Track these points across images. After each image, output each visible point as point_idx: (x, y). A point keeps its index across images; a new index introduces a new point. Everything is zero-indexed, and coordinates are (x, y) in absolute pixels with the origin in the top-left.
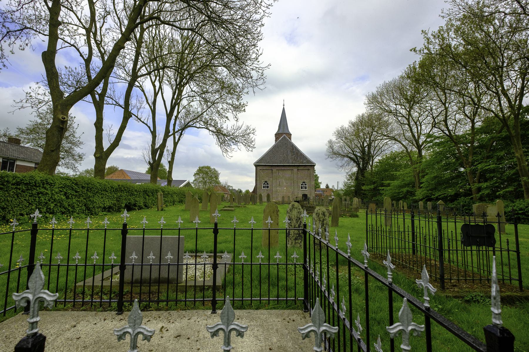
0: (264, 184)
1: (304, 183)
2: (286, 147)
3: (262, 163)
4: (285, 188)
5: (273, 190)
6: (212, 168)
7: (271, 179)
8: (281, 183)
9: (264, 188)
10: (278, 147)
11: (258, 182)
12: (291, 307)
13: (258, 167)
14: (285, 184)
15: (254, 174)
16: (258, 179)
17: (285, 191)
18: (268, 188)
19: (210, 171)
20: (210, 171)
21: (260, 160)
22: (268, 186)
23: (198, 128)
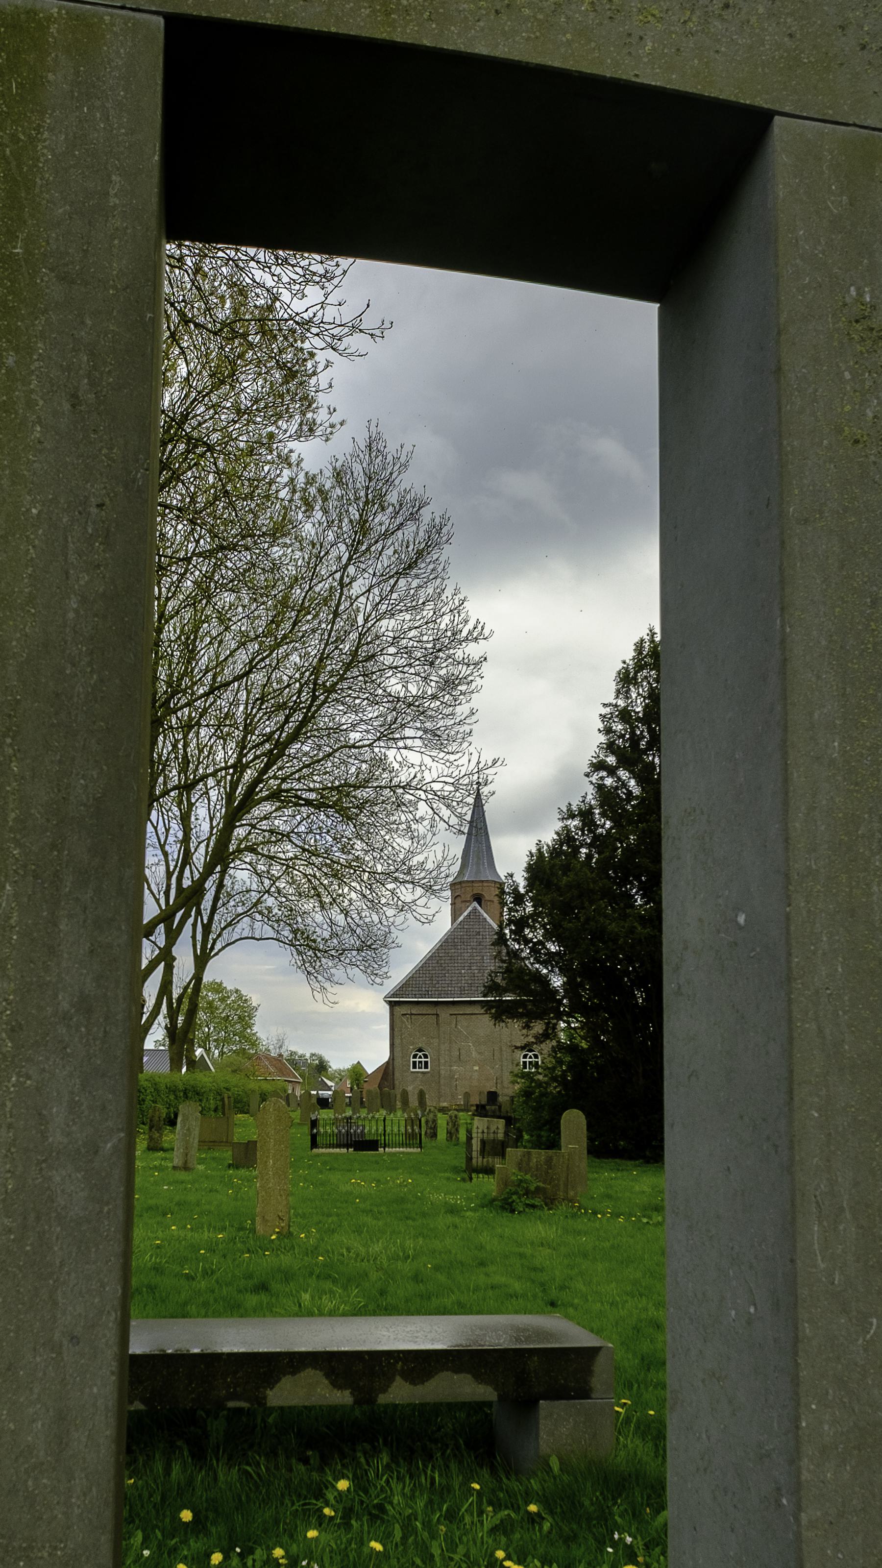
0: (415, 1056)
1: (420, 1050)
2: (480, 944)
3: (407, 996)
4: (476, 1068)
5: (442, 1072)
6: (229, 986)
7: (435, 1041)
8: (463, 1052)
9: (414, 1067)
10: (455, 946)
11: (397, 1049)
12: (448, 1301)
13: (397, 1009)
14: (474, 1054)
15: (385, 1028)
16: (397, 1041)
17: (476, 1076)
18: (426, 1067)
19: (223, 1000)
20: (223, 1000)
21: (408, 980)
22: (426, 1063)
23: (258, 940)
